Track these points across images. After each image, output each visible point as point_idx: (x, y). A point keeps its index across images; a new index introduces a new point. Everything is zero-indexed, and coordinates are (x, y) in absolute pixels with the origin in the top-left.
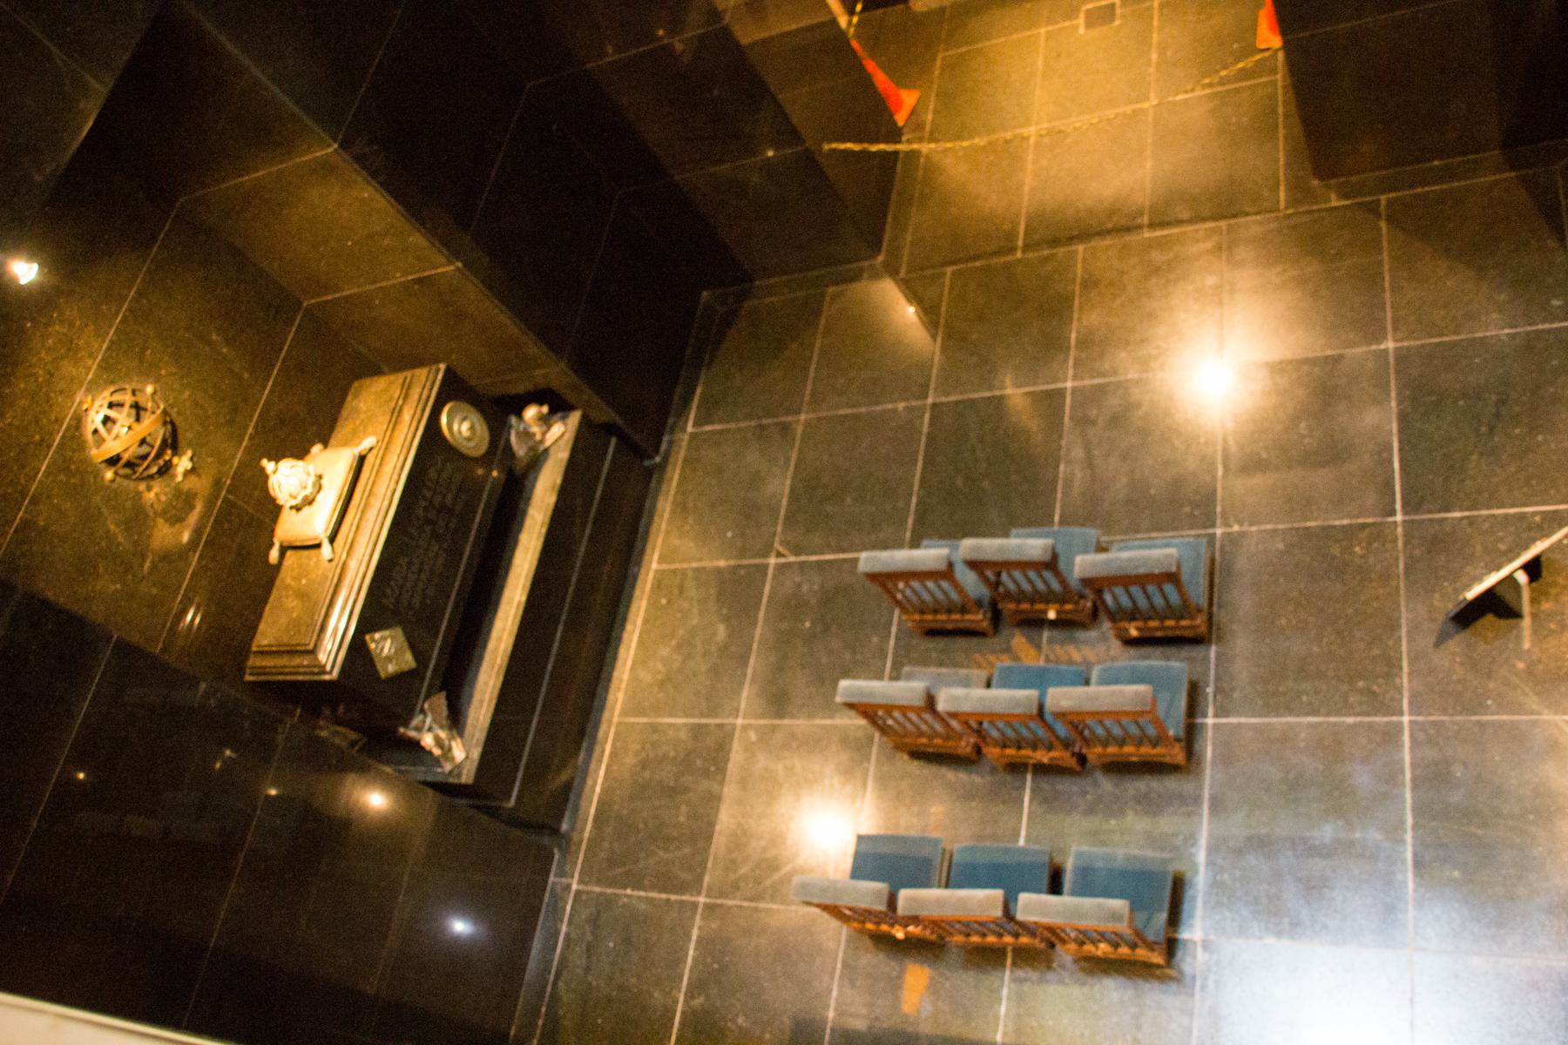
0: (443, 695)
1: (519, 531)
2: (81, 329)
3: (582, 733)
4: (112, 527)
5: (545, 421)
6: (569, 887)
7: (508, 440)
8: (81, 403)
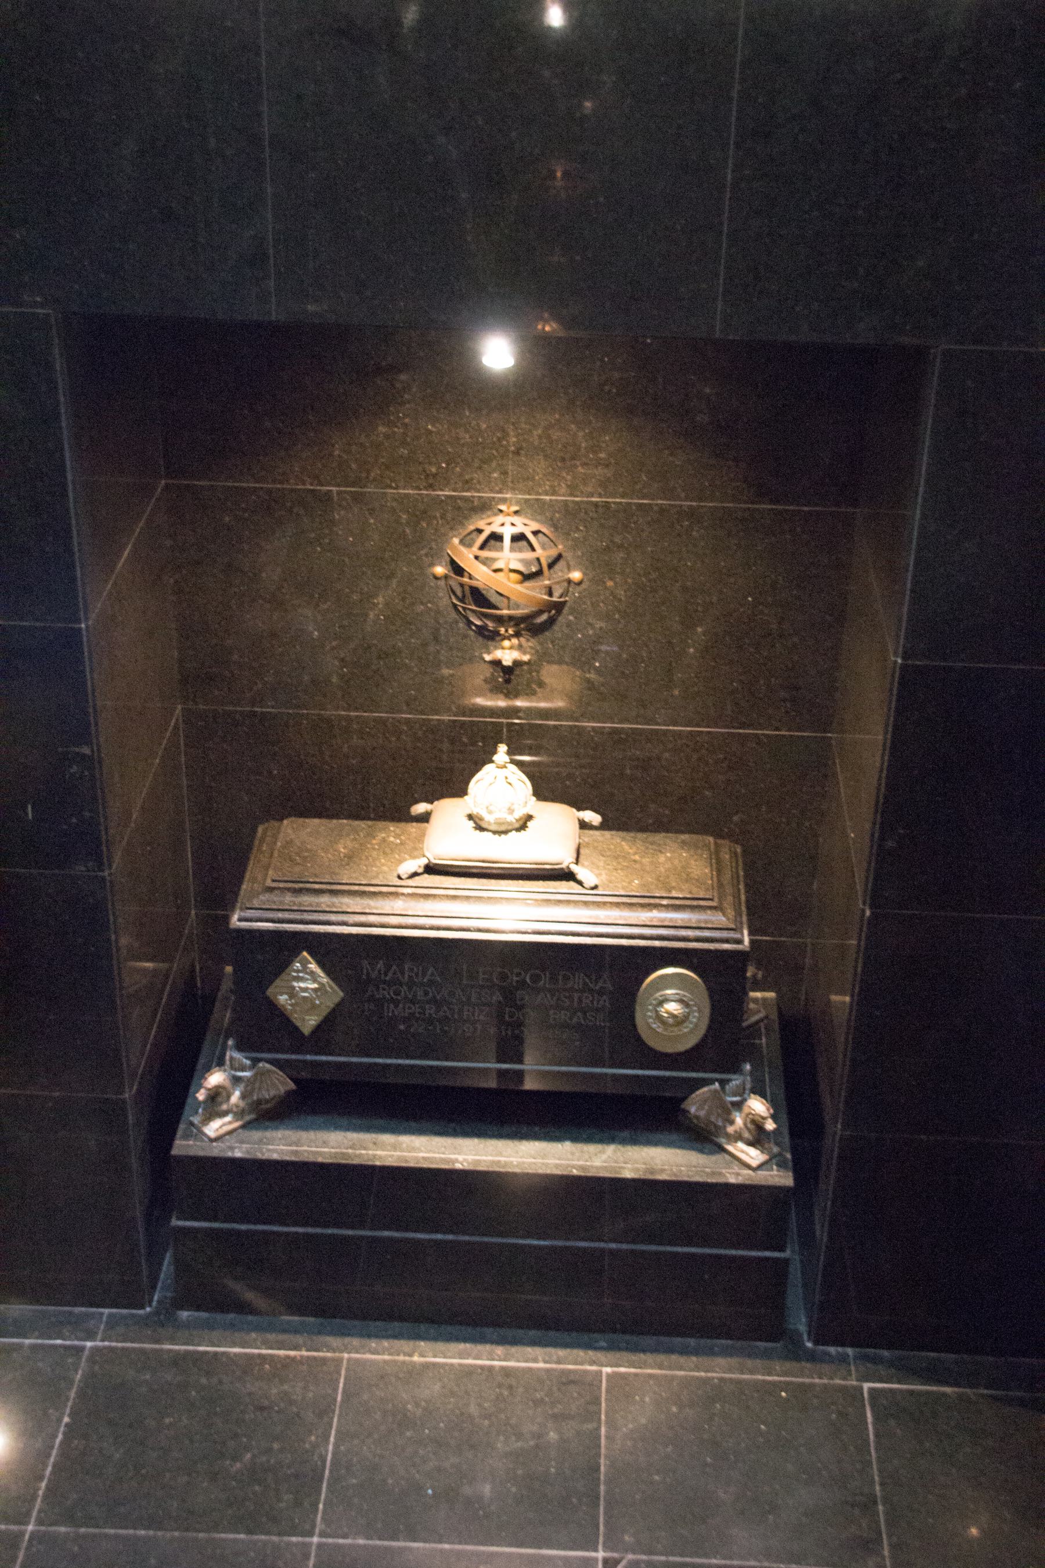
0: (292, 1086)
1: (575, 1140)
2: (598, 463)
3: (321, 1312)
4: (380, 600)
5: (758, 1137)
6: (90, 1336)
8: (504, 501)
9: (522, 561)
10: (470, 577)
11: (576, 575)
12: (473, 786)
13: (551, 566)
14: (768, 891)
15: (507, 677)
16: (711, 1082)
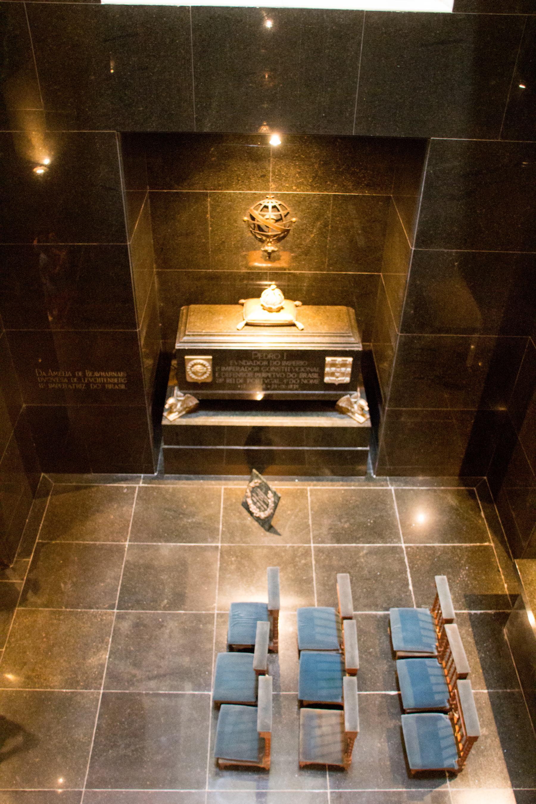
7: (344, 395)
9: (275, 215)
10: (258, 221)
11: (294, 220)
12: (263, 294)
13: (285, 216)
14: (367, 328)
15: (269, 256)
16: (346, 394)
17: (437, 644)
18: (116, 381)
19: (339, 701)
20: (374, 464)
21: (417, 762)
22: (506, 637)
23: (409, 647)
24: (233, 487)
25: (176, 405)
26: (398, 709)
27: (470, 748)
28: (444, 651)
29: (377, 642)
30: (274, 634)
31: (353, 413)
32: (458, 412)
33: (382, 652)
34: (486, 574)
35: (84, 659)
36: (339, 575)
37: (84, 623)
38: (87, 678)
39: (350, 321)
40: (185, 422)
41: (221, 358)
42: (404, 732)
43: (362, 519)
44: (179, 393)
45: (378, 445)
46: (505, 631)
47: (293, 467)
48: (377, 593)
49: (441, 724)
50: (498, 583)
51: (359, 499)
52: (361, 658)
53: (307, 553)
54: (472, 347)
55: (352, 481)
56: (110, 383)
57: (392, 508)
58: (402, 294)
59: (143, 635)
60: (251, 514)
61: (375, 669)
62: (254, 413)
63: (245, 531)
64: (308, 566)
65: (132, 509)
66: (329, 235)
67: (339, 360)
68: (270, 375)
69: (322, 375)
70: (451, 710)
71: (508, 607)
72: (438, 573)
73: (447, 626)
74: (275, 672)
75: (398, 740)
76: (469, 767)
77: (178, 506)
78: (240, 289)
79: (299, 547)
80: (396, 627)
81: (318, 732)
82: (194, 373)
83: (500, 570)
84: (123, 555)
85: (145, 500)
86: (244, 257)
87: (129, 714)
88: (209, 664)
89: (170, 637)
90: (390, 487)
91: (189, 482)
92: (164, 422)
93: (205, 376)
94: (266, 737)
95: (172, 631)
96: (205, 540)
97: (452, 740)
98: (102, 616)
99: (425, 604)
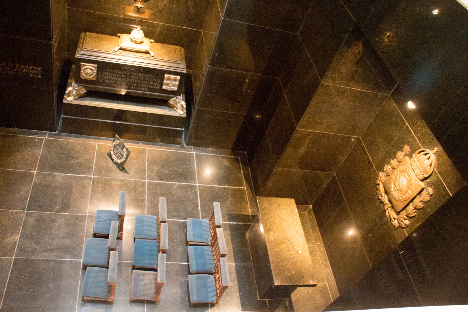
0: (86, 91)
7: (173, 97)
12: (132, 32)
15: (138, 10)
16: (174, 97)
17: (211, 239)
18: (35, 73)
19: (155, 267)
20: (185, 139)
21: (194, 299)
22: (247, 237)
23: (196, 240)
24: (105, 144)
25: (73, 92)
26: (187, 272)
27: (223, 292)
28: (214, 243)
29: (178, 236)
30: (121, 229)
31: (177, 108)
32: (235, 114)
33: (181, 242)
34: (241, 203)
35: (3, 239)
36: (161, 198)
37: (5, 218)
38: (4, 250)
39: (181, 55)
40: (77, 102)
41: (103, 67)
42: (189, 283)
43: (176, 169)
44: (75, 85)
45: (189, 128)
46: (247, 234)
47: (139, 136)
48: (181, 210)
49: (209, 280)
50: (246, 209)
51: (175, 157)
52: (169, 244)
53: (143, 184)
54: (247, 80)
55: (172, 147)
56: (32, 73)
57: (193, 164)
58: (213, 44)
59: (42, 226)
60: (113, 160)
61: (176, 251)
62: (119, 102)
63: (108, 170)
64: (143, 192)
65: (40, 152)
66: (175, 3)
67: (172, 77)
68: (131, 80)
69: (162, 84)
70: (215, 273)
71: (250, 221)
72: (215, 201)
73: (217, 229)
74: (120, 250)
75: (185, 288)
76: (221, 301)
77: (69, 152)
78: (120, 27)
79: (139, 181)
80: (189, 228)
81: (142, 283)
82: (85, 73)
83: (248, 202)
84: (33, 179)
85: (49, 147)
86: (123, 9)
87: (31, 271)
88: (82, 244)
89: (59, 228)
90: (193, 152)
91: (77, 139)
92: (64, 101)
93: (92, 76)
94: (112, 284)
95: (60, 224)
96: (84, 173)
97: (214, 288)
98: (17, 214)
99: (206, 217)
